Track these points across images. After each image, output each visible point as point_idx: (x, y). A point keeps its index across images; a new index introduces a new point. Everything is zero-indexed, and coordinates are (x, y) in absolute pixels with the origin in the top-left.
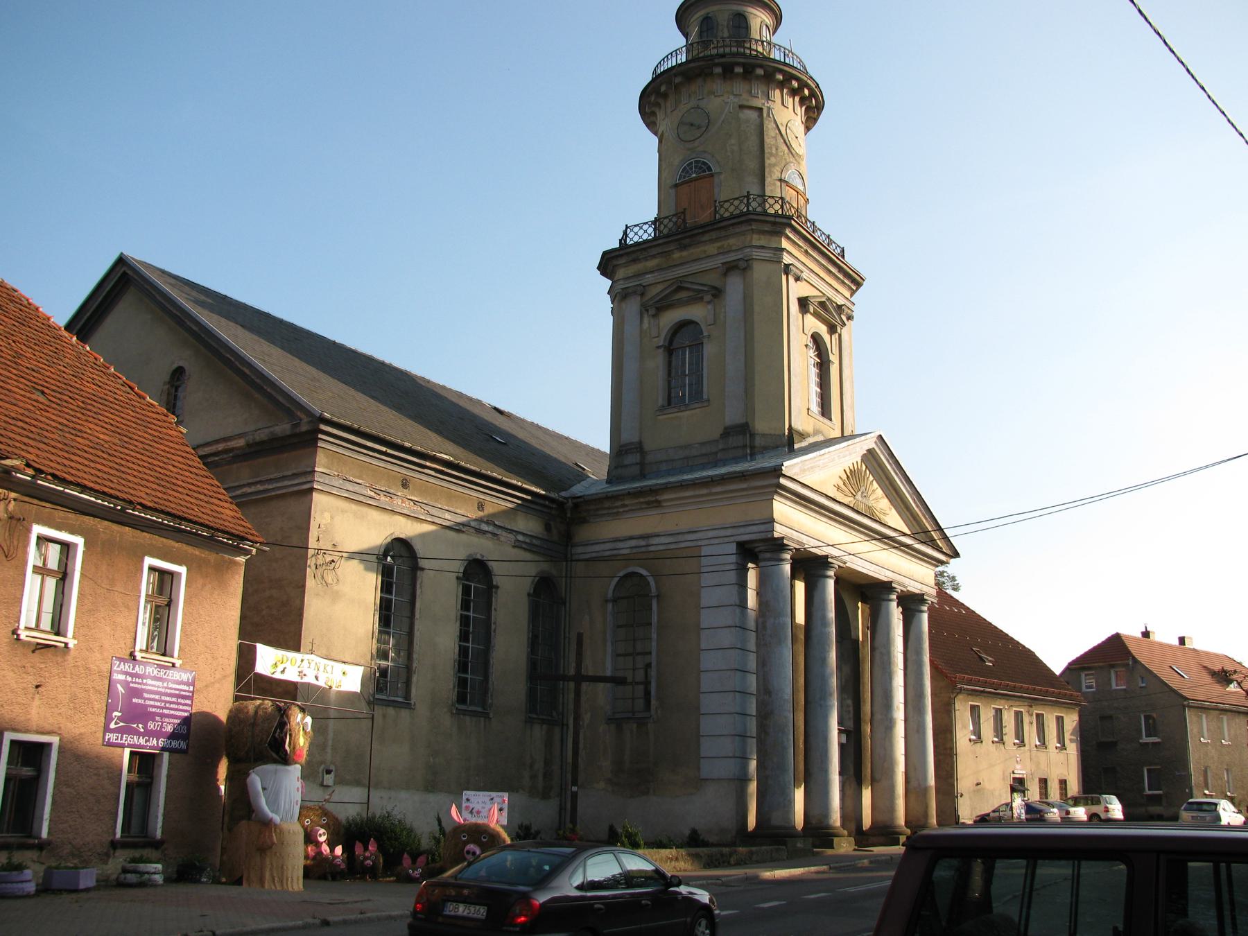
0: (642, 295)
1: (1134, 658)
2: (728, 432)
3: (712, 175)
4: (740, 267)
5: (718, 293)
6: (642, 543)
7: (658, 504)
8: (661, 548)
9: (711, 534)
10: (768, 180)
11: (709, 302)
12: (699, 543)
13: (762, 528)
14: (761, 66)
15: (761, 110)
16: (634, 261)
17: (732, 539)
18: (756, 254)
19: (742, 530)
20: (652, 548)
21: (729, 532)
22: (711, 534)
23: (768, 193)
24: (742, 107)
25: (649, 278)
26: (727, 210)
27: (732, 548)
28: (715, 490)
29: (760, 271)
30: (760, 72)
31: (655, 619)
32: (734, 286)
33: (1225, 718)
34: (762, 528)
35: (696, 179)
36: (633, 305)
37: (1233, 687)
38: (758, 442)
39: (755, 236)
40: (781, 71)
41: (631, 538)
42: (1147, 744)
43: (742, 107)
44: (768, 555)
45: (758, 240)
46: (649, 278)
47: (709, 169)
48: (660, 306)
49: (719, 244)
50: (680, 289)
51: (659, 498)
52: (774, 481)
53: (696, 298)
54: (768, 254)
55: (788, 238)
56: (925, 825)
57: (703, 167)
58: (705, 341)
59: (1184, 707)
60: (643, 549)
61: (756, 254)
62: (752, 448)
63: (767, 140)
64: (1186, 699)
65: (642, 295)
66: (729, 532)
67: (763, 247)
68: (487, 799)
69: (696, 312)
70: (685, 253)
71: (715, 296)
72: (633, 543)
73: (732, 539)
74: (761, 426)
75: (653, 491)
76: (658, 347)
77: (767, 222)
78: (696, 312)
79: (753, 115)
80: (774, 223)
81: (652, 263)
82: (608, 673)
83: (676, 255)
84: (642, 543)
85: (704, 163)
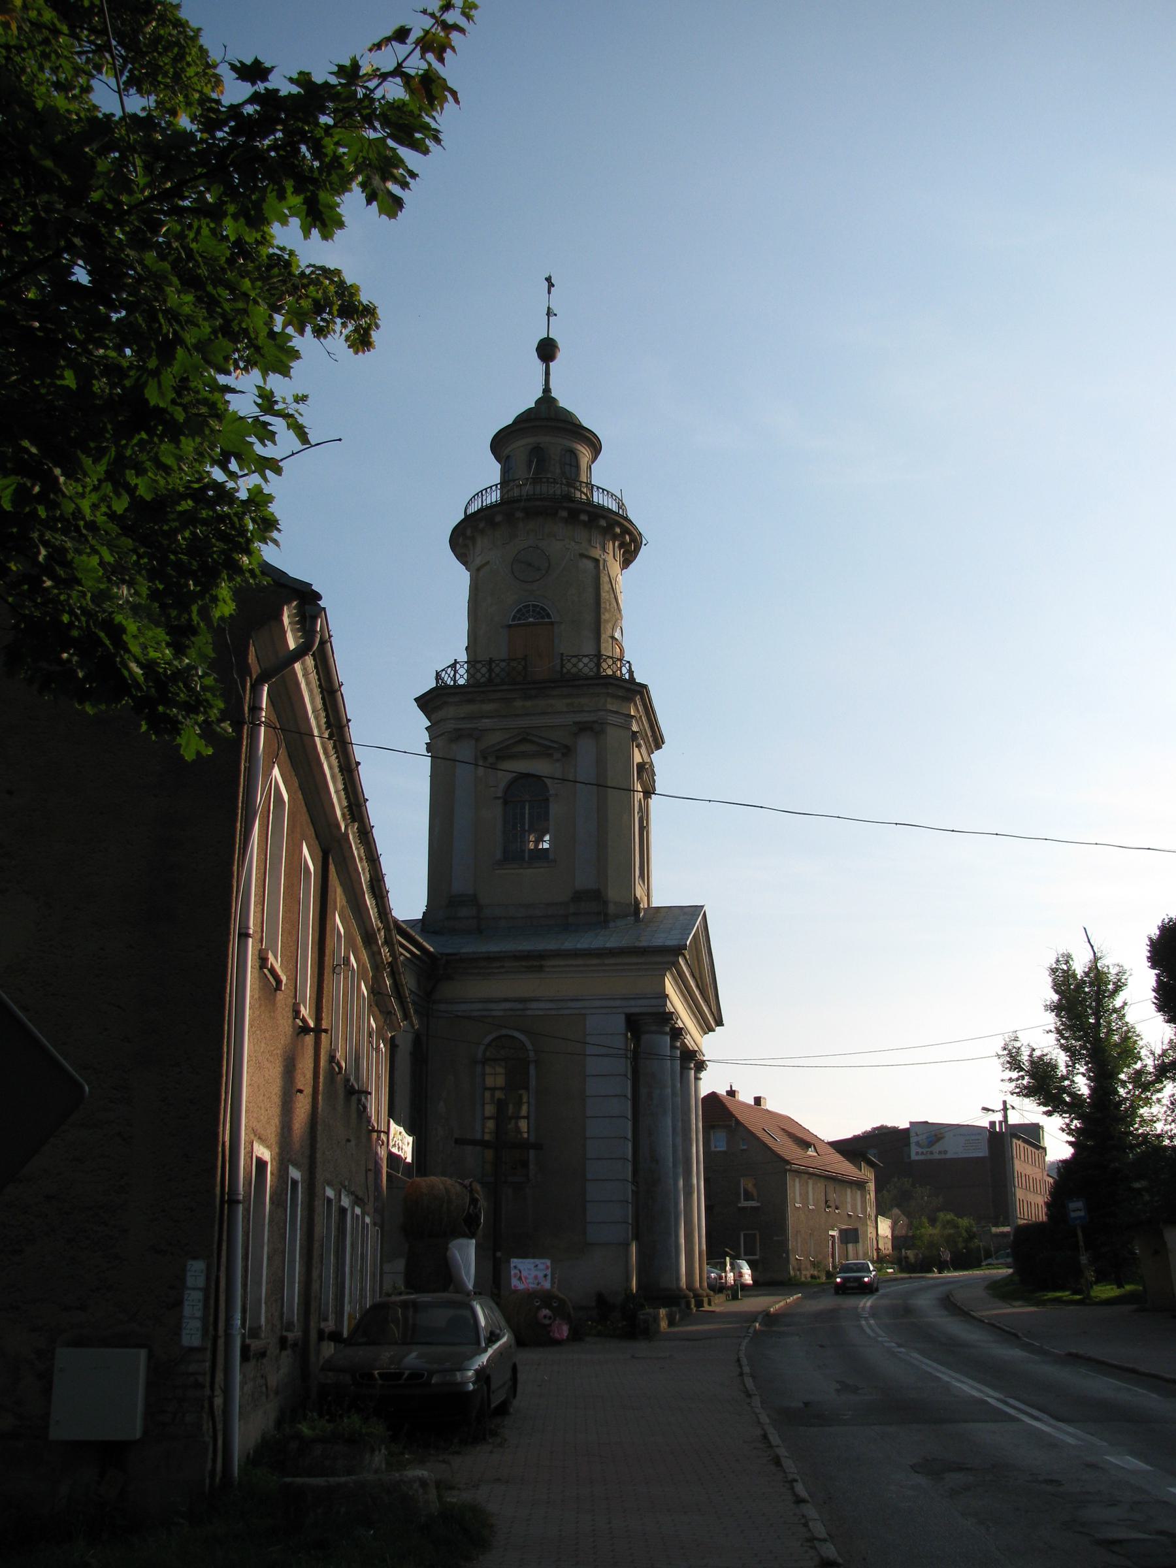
0: (477, 740)
1: (737, 1120)
2: (579, 896)
3: (552, 624)
4: (593, 729)
5: (567, 751)
6: (520, 1006)
7: (540, 969)
8: (541, 1013)
9: (598, 1003)
10: (603, 636)
11: (558, 760)
12: (583, 1011)
13: (654, 1002)
14: (604, 517)
15: (597, 561)
16: (470, 701)
17: (620, 1010)
18: (612, 719)
19: (632, 1003)
20: (529, 1013)
21: (618, 1003)
22: (598, 1003)
23: (603, 652)
24: (582, 556)
25: (486, 723)
26: (575, 665)
27: (620, 1023)
28: (607, 961)
29: (613, 735)
30: (603, 523)
31: (533, 1083)
32: (586, 747)
33: (811, 1182)
34: (654, 1002)
35: (533, 624)
36: (465, 751)
37: (811, 1152)
38: (612, 909)
39: (609, 700)
40: (604, 517)
41: (506, 1000)
42: (744, 1208)
43: (582, 556)
44: (654, 1028)
45: (612, 705)
46: (486, 723)
47: (549, 616)
48: (502, 754)
49: (569, 701)
50: (524, 740)
51: (543, 963)
52: (671, 959)
53: (545, 752)
54: (619, 720)
55: (636, 705)
56: (1007, 1280)
57: (542, 613)
58: (551, 799)
59: (786, 1171)
60: (519, 1013)
61: (612, 719)
62: (606, 915)
63: (603, 594)
64: (788, 1162)
65: (477, 740)
66: (618, 1003)
67: (616, 712)
68: (532, 1266)
69: (540, 767)
70: (529, 704)
71: (564, 755)
72: (508, 1005)
73: (620, 1010)
74: (612, 894)
75: (542, 956)
76: (498, 798)
77: (622, 687)
78: (540, 767)
79: (590, 565)
80: (628, 690)
81: (488, 707)
82: (478, 1136)
83: (519, 703)
84: (520, 1006)
85: (543, 609)
